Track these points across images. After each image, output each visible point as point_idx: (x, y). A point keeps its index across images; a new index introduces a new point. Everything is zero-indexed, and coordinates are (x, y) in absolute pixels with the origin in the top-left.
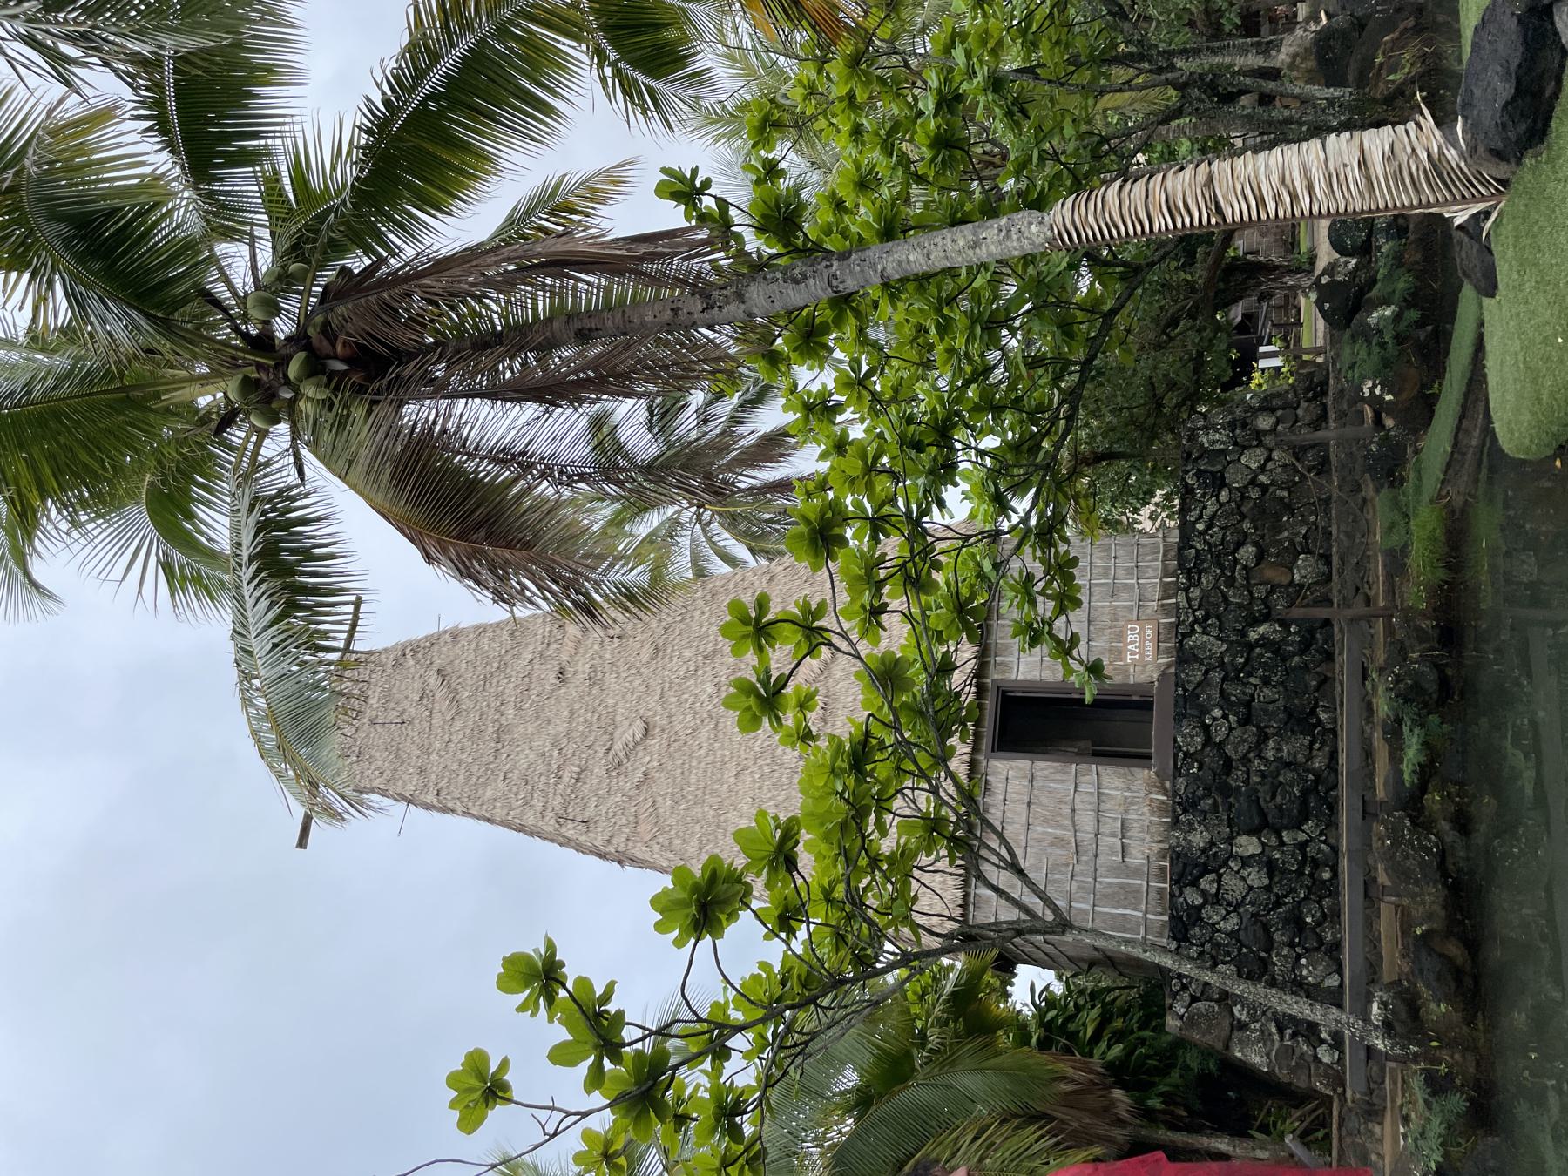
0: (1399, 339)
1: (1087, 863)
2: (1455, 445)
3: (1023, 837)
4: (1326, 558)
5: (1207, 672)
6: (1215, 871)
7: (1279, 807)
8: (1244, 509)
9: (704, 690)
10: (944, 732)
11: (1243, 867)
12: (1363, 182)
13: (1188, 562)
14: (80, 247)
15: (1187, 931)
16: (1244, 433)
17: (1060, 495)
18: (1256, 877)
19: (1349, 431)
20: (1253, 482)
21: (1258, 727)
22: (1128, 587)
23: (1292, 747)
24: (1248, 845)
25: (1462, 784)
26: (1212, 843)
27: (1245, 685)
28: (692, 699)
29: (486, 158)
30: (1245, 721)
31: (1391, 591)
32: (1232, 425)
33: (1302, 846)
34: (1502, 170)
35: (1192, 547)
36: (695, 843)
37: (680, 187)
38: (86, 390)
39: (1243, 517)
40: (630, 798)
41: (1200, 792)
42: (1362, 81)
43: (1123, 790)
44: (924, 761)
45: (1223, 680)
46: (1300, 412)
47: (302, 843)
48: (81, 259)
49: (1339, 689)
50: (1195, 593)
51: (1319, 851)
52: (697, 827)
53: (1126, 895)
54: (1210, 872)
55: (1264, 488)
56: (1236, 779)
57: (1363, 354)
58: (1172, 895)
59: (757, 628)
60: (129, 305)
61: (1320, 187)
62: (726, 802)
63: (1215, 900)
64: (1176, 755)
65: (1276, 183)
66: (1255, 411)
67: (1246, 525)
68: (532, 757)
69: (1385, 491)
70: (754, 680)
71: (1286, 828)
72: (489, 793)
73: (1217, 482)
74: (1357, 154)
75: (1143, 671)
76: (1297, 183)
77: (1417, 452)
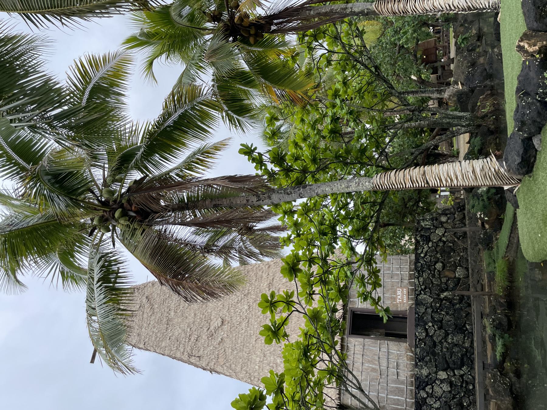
0: (489, 199)
1: (384, 378)
2: (509, 241)
3: (361, 368)
4: (467, 269)
5: (426, 309)
6: (431, 384)
7: (454, 361)
8: (438, 249)
9: (244, 308)
10: (333, 334)
11: (441, 383)
12: (473, 177)
13: (418, 269)
14: (53, 181)
15: (421, 407)
16: (437, 223)
17: (373, 247)
18: (446, 387)
19: (473, 229)
20: (440, 240)
21: (445, 331)
22: (397, 275)
23: (458, 338)
24: (442, 375)
25: (517, 360)
26: (430, 374)
27: (440, 314)
28: (239, 311)
29: (184, 144)
30: (440, 328)
31: (490, 286)
32: (432, 219)
33: (462, 376)
34: (519, 177)
35: (420, 262)
36: (239, 366)
37: (247, 150)
38: (46, 221)
39: (437, 252)
40: (216, 348)
41: (425, 354)
42: (473, 111)
43: (397, 351)
44: (327, 347)
45: (432, 312)
46: (456, 216)
47: (92, 361)
48: (53, 184)
49: (473, 318)
50: (421, 279)
51: (468, 378)
52: (241, 360)
53: (399, 392)
54: (429, 385)
55: (444, 242)
56: (438, 350)
57: (477, 203)
58: (416, 393)
59: (271, 304)
60: (66, 196)
61: (460, 178)
62: (252, 351)
63: (431, 395)
64: (416, 340)
65: (446, 176)
66: (440, 215)
67: (439, 255)
68: (180, 331)
69: (486, 251)
70: (270, 324)
71: (456, 369)
72: (163, 344)
73: (428, 240)
74: (471, 169)
75: (403, 306)
76: (452, 176)
77: (497, 239)
